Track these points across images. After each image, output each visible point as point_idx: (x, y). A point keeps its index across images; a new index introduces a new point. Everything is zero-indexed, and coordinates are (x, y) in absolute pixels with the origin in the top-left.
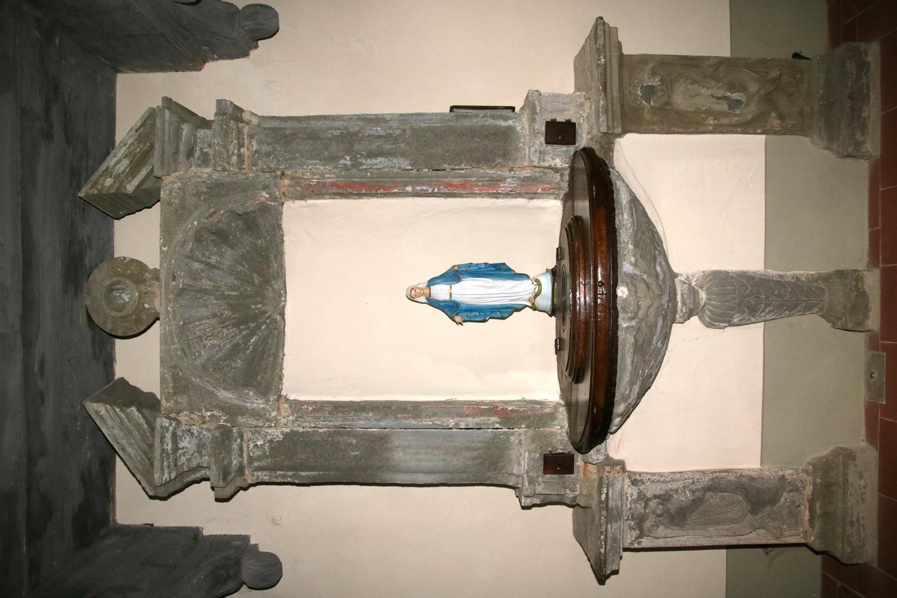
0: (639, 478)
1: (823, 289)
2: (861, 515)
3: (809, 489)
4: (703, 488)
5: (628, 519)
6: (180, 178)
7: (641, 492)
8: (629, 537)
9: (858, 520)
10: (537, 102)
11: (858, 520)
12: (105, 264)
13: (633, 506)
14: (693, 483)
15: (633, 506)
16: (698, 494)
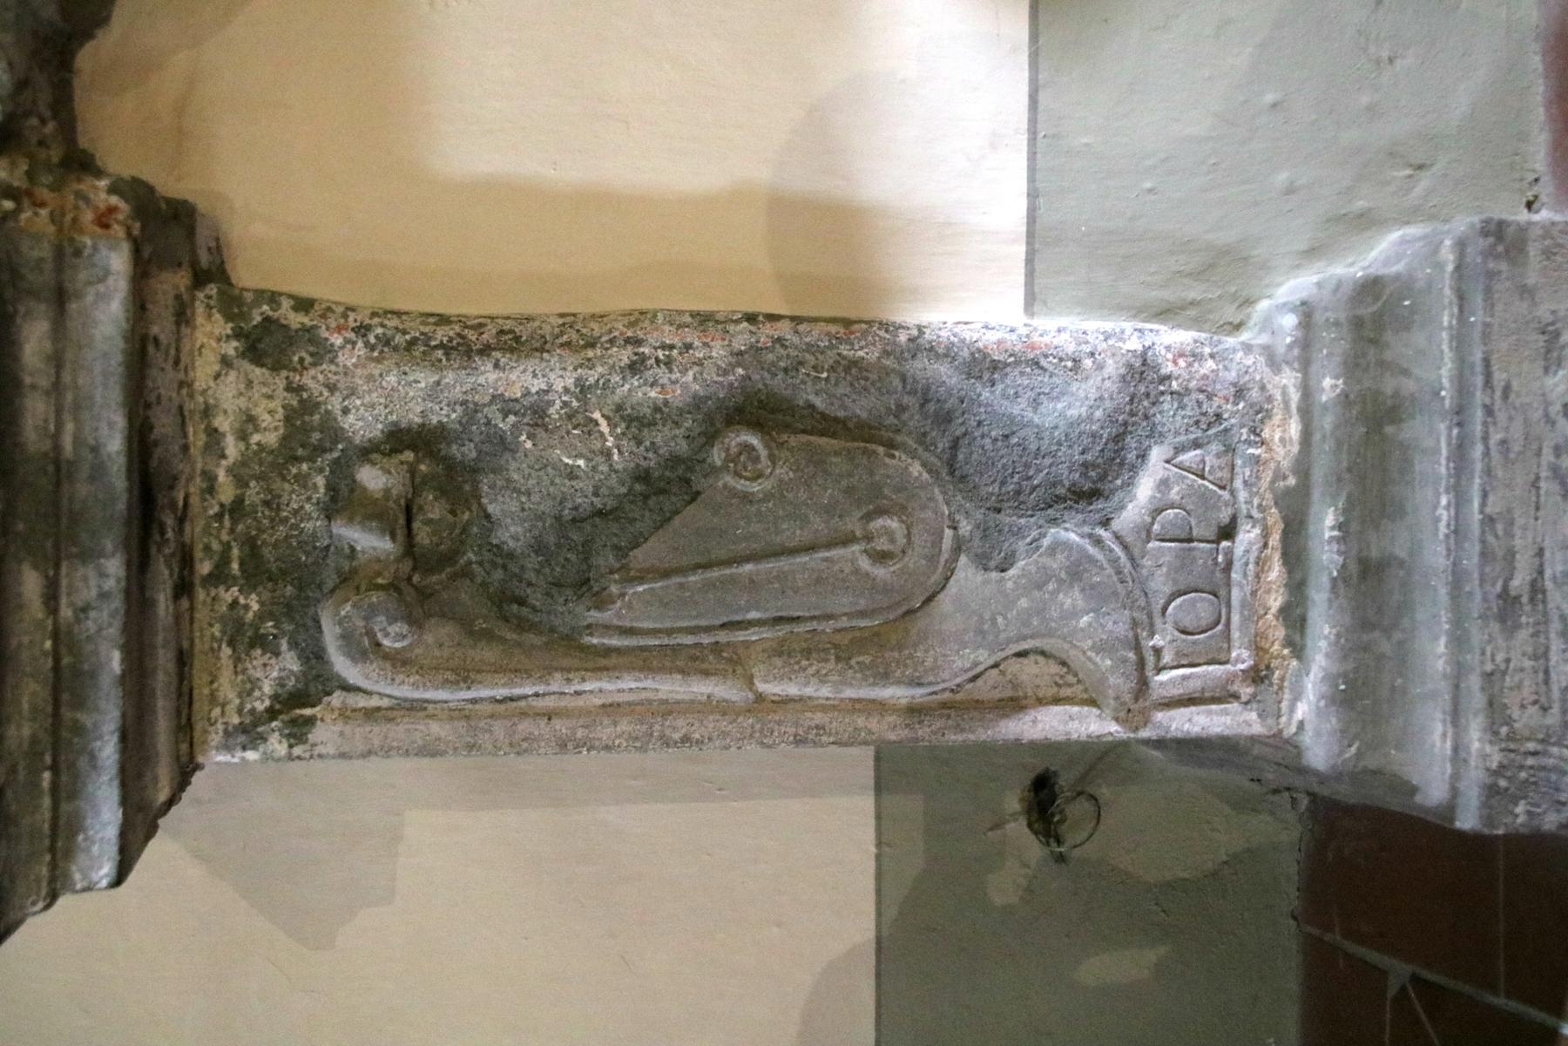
0: (296, 320)
1: (1137, 729)
2: (1555, 566)
3: (1284, 434)
4: (697, 403)
5: (219, 576)
6: (1244, 465)
7: (309, 406)
8: (227, 688)
9: (1536, 589)
10: (1072, 279)
11: (1536, 589)
12: (1518, 556)
13: (254, 494)
14: (636, 367)
15: (254, 494)
16: (670, 439)
